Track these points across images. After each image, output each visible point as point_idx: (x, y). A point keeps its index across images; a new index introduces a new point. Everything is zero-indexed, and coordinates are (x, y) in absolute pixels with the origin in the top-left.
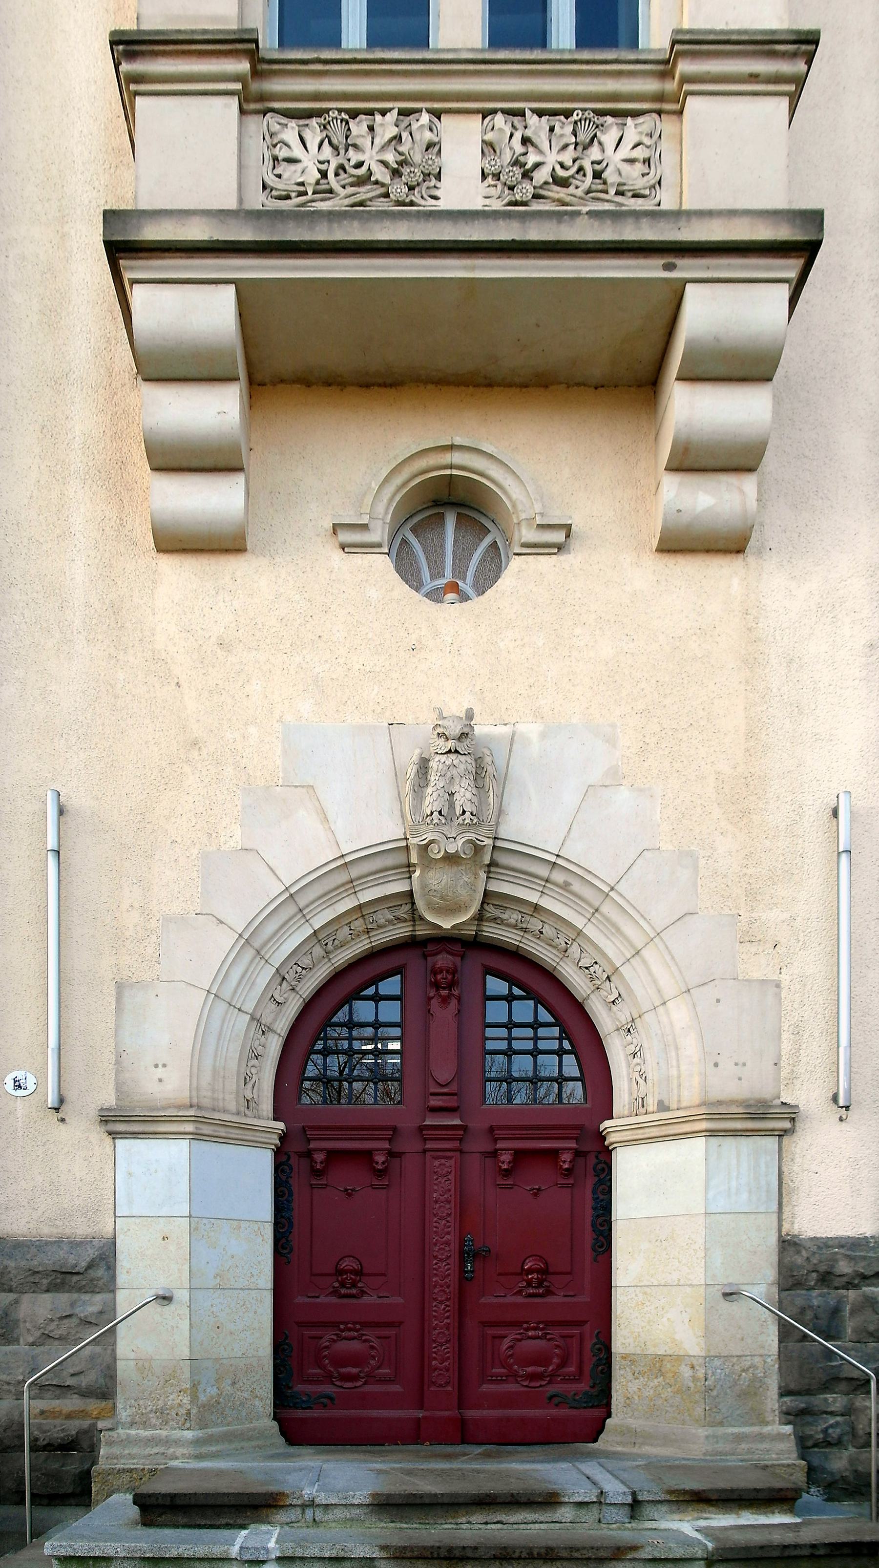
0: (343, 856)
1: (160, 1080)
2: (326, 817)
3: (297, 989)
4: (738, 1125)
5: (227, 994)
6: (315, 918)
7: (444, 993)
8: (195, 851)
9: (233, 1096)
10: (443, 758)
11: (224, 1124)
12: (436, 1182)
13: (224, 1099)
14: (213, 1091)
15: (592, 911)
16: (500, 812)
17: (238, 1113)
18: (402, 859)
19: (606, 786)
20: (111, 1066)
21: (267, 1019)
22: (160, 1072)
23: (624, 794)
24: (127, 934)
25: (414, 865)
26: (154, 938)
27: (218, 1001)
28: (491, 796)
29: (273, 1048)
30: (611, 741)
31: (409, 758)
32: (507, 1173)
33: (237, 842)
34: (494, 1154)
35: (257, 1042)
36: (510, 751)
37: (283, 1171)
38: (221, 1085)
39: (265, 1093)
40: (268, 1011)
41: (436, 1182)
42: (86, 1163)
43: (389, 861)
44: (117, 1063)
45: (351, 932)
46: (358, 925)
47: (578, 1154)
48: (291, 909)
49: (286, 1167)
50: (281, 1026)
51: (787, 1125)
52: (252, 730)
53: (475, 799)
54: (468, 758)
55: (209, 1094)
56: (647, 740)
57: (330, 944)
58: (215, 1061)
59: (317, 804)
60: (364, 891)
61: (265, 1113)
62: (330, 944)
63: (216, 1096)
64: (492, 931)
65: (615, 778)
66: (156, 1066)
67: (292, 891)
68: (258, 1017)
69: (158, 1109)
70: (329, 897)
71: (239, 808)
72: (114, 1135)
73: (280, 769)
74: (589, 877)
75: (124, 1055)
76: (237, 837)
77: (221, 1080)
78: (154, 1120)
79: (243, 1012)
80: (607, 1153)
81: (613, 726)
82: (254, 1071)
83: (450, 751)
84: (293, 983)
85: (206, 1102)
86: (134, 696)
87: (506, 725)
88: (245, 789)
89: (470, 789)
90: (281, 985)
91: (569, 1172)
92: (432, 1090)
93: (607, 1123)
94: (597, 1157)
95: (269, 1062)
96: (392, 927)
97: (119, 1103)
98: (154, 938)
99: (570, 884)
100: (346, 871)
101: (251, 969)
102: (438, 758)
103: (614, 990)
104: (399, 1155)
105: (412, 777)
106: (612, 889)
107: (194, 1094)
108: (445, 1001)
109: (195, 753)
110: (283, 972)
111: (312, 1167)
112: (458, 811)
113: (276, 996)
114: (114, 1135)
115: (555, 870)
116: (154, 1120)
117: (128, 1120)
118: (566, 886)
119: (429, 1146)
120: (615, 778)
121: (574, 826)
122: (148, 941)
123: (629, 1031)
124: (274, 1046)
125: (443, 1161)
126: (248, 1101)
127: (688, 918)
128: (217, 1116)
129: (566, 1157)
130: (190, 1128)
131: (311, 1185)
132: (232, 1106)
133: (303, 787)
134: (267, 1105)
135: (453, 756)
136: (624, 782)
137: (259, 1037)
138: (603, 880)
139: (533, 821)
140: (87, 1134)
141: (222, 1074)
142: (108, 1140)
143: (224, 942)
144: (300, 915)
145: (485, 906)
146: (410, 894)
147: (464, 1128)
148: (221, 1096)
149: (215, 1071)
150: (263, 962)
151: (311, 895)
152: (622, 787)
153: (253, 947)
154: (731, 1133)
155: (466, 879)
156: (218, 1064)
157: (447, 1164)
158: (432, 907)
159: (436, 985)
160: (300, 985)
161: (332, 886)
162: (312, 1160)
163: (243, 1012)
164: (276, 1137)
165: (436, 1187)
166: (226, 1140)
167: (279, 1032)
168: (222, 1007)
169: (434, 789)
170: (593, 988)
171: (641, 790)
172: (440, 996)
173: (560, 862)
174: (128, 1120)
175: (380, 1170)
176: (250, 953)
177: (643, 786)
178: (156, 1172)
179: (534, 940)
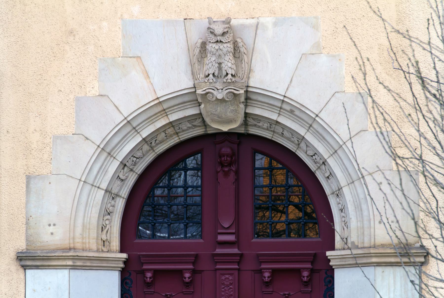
0: (158, 98)
1: (52, 234)
2: (148, 75)
3: (134, 170)
4: (393, 260)
5: (90, 180)
6: (143, 131)
7: (226, 169)
8: (72, 97)
9: (95, 241)
10: (214, 45)
11: (90, 259)
12: (223, 290)
13: (89, 242)
14: (83, 238)
15: (308, 126)
16: (250, 70)
17: (98, 251)
18: (193, 98)
19: (313, 54)
20: (24, 226)
21: (115, 191)
22: (52, 229)
23: (323, 59)
24: (33, 146)
25: (201, 103)
26: (48, 148)
27: (86, 184)
28: (244, 63)
29: (119, 207)
30: (315, 27)
31: (196, 38)
32: (267, 284)
33: (95, 92)
34: (260, 272)
35: (109, 205)
36: (256, 34)
37: (126, 283)
38: (87, 234)
39: (115, 235)
40: (116, 185)
41: (223, 290)
42: (9, 283)
43: (186, 99)
44: (27, 224)
45: (166, 135)
46: (170, 131)
47: (312, 271)
48: (129, 128)
49: (211, 95)
50: (124, 192)
51: (422, 260)
52: (105, 24)
53: (234, 67)
54: (228, 45)
55: (80, 240)
56: (337, 26)
57: (153, 143)
58: (84, 220)
59: (142, 67)
60: (172, 114)
61: (115, 248)
62: (153, 143)
63: (84, 241)
64: (253, 131)
65: (317, 49)
66: (50, 225)
67: (129, 119)
68: (110, 189)
69: (51, 252)
70: (151, 120)
71: (97, 71)
72: (25, 268)
73: (121, 47)
74: (303, 109)
75: (31, 219)
76: (96, 88)
77: (87, 231)
78: (48, 259)
79: (101, 189)
80: (330, 271)
81: (316, 18)
82: (107, 222)
83: (217, 41)
84: (131, 167)
85: (78, 246)
86: (35, 4)
87: (253, 18)
88: (101, 59)
89: (230, 61)
90: (123, 169)
91: (306, 284)
92: (219, 231)
93: (328, 253)
94: (326, 273)
95: (117, 215)
96: (192, 130)
97: (28, 248)
98: (48, 148)
99: (294, 111)
100: (161, 107)
101: (105, 164)
102: (211, 45)
103: (327, 170)
104: (201, 272)
105: (197, 54)
106: (317, 116)
107: (71, 241)
108: (226, 174)
109: (72, 38)
110: (125, 162)
111: (145, 280)
112: (224, 73)
113: (121, 176)
114: (25, 268)
115: (284, 105)
116: (48, 259)
117: (34, 258)
118: (292, 112)
119: (218, 267)
120: (317, 49)
121: (294, 79)
122: (44, 150)
123: (338, 195)
124: (120, 204)
125: (227, 276)
126: (104, 241)
127: (362, 133)
128: (85, 254)
129: (305, 274)
130: (70, 263)
131: (145, 292)
132: (94, 247)
133: (134, 57)
134: (116, 243)
135: (220, 44)
136: (323, 51)
137: (110, 201)
138: (311, 111)
139: (269, 75)
140: (9, 267)
141: (88, 227)
142: (22, 270)
143: (89, 150)
144: (134, 131)
145: (248, 119)
146: (201, 114)
147: (241, 255)
148: (87, 241)
149: (83, 225)
150: (112, 158)
151: (140, 120)
152: (322, 55)
153: (106, 152)
154: (389, 264)
155: (232, 108)
156: (85, 221)
157: (230, 278)
158: (213, 120)
159: (222, 164)
160: (136, 167)
161: (152, 114)
162: (145, 276)
163: (101, 189)
164: (121, 263)
165: (223, 293)
166: (91, 268)
167: (123, 196)
168: (88, 187)
169: (210, 61)
170: (317, 167)
171: (334, 56)
172: (224, 171)
173: (286, 100)
174: (34, 258)
175: (187, 283)
176: (105, 155)
177: (335, 54)
178: (49, 289)
179: (280, 137)
